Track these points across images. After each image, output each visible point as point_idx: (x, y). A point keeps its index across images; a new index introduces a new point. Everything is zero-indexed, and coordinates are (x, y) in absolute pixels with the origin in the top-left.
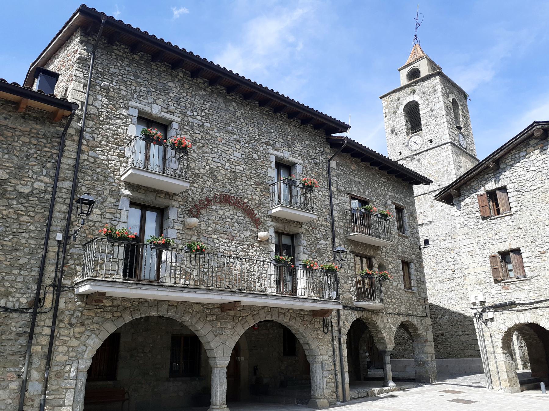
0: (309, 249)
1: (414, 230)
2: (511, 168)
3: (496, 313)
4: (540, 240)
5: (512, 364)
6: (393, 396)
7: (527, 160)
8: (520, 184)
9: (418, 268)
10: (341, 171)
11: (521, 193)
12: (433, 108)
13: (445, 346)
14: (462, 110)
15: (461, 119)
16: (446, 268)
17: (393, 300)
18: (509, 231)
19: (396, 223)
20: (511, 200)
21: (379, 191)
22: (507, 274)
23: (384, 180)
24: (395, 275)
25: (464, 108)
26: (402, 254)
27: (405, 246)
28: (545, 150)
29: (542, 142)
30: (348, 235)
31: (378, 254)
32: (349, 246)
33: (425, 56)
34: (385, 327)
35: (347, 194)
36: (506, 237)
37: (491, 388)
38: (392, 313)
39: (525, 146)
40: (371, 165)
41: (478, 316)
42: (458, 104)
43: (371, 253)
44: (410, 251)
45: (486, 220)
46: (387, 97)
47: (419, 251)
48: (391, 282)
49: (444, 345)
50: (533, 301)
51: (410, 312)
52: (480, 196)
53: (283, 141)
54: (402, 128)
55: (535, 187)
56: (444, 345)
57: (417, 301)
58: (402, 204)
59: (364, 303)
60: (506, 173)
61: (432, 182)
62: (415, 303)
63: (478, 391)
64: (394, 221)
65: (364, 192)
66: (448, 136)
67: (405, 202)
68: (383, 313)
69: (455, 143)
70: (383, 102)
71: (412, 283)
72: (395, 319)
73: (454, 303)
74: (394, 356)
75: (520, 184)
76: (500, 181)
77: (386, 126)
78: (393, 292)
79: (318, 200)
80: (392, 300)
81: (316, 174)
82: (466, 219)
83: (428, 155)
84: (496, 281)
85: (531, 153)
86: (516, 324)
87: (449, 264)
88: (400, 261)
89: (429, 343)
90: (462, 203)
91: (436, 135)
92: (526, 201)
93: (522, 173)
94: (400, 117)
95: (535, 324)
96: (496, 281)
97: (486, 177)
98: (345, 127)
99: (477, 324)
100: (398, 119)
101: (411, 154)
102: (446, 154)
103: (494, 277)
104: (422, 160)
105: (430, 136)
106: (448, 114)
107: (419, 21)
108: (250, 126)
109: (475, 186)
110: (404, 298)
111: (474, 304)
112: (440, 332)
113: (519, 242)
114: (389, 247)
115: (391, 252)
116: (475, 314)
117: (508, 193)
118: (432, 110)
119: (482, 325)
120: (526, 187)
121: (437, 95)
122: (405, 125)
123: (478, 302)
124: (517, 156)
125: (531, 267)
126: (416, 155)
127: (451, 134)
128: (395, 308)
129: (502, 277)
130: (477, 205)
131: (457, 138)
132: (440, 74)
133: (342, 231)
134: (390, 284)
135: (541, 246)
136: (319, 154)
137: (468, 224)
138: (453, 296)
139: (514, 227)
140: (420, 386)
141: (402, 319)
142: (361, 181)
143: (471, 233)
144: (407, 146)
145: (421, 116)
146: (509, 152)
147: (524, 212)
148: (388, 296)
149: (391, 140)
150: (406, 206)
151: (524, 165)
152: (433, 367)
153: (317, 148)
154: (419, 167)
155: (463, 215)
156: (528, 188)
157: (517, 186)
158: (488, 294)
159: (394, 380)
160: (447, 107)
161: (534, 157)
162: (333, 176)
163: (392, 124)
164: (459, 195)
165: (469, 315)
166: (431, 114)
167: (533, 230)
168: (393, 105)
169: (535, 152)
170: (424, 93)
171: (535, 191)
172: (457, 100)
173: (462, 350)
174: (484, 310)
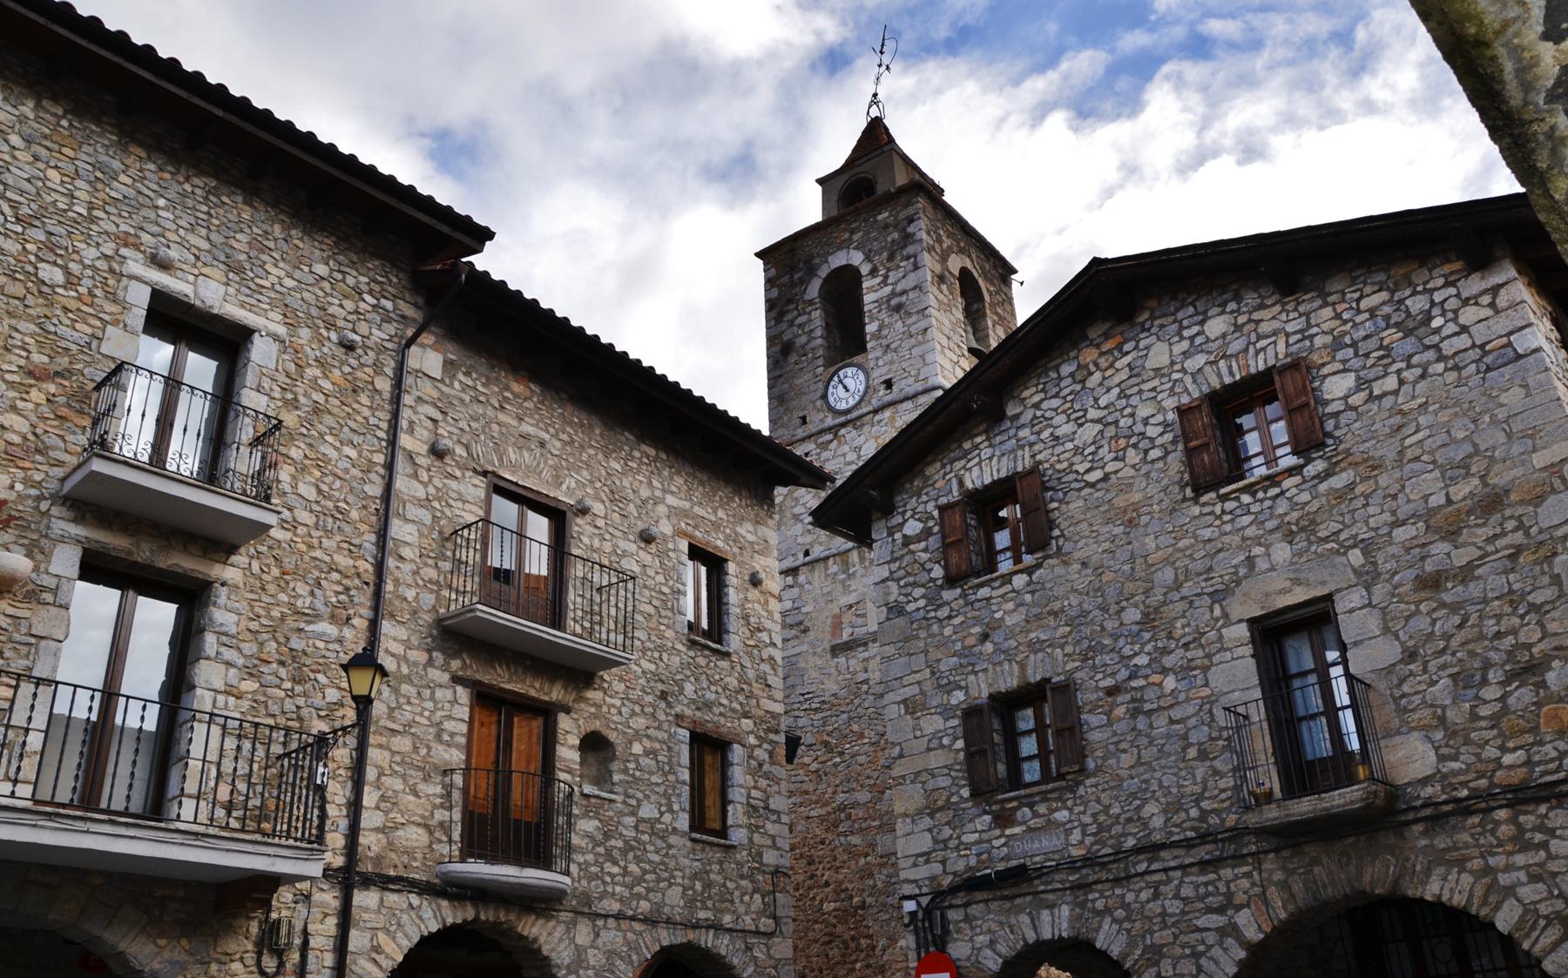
0: (249, 648)
8: (1058, 467)
9: (761, 765)
10: (463, 390)
17: (633, 867)
18: (1023, 624)
24: (654, 779)
26: (698, 709)
29: (1119, 329)
35: (475, 471)
38: (619, 916)
42: (979, 288)
48: (634, 802)
51: (702, 915)
53: (205, 245)
57: (742, 877)
58: (720, 543)
62: (729, 884)
65: (557, 477)
67: (735, 538)
71: (730, 814)
79: (335, 475)
80: (625, 868)
81: (341, 382)
86: (1026, 944)
88: (684, 734)
93: (1067, 429)
94: (810, 313)
97: (967, 445)
105: (885, 369)
108: (56, 167)
109: (936, 477)
113: (1047, 660)
115: (649, 699)
120: (1075, 476)
124: (1054, 375)
128: (639, 897)
130: (934, 542)
136: (368, 316)
141: (666, 937)
150: (736, 550)
151: (1069, 405)
153: (367, 297)
172: (976, 275)
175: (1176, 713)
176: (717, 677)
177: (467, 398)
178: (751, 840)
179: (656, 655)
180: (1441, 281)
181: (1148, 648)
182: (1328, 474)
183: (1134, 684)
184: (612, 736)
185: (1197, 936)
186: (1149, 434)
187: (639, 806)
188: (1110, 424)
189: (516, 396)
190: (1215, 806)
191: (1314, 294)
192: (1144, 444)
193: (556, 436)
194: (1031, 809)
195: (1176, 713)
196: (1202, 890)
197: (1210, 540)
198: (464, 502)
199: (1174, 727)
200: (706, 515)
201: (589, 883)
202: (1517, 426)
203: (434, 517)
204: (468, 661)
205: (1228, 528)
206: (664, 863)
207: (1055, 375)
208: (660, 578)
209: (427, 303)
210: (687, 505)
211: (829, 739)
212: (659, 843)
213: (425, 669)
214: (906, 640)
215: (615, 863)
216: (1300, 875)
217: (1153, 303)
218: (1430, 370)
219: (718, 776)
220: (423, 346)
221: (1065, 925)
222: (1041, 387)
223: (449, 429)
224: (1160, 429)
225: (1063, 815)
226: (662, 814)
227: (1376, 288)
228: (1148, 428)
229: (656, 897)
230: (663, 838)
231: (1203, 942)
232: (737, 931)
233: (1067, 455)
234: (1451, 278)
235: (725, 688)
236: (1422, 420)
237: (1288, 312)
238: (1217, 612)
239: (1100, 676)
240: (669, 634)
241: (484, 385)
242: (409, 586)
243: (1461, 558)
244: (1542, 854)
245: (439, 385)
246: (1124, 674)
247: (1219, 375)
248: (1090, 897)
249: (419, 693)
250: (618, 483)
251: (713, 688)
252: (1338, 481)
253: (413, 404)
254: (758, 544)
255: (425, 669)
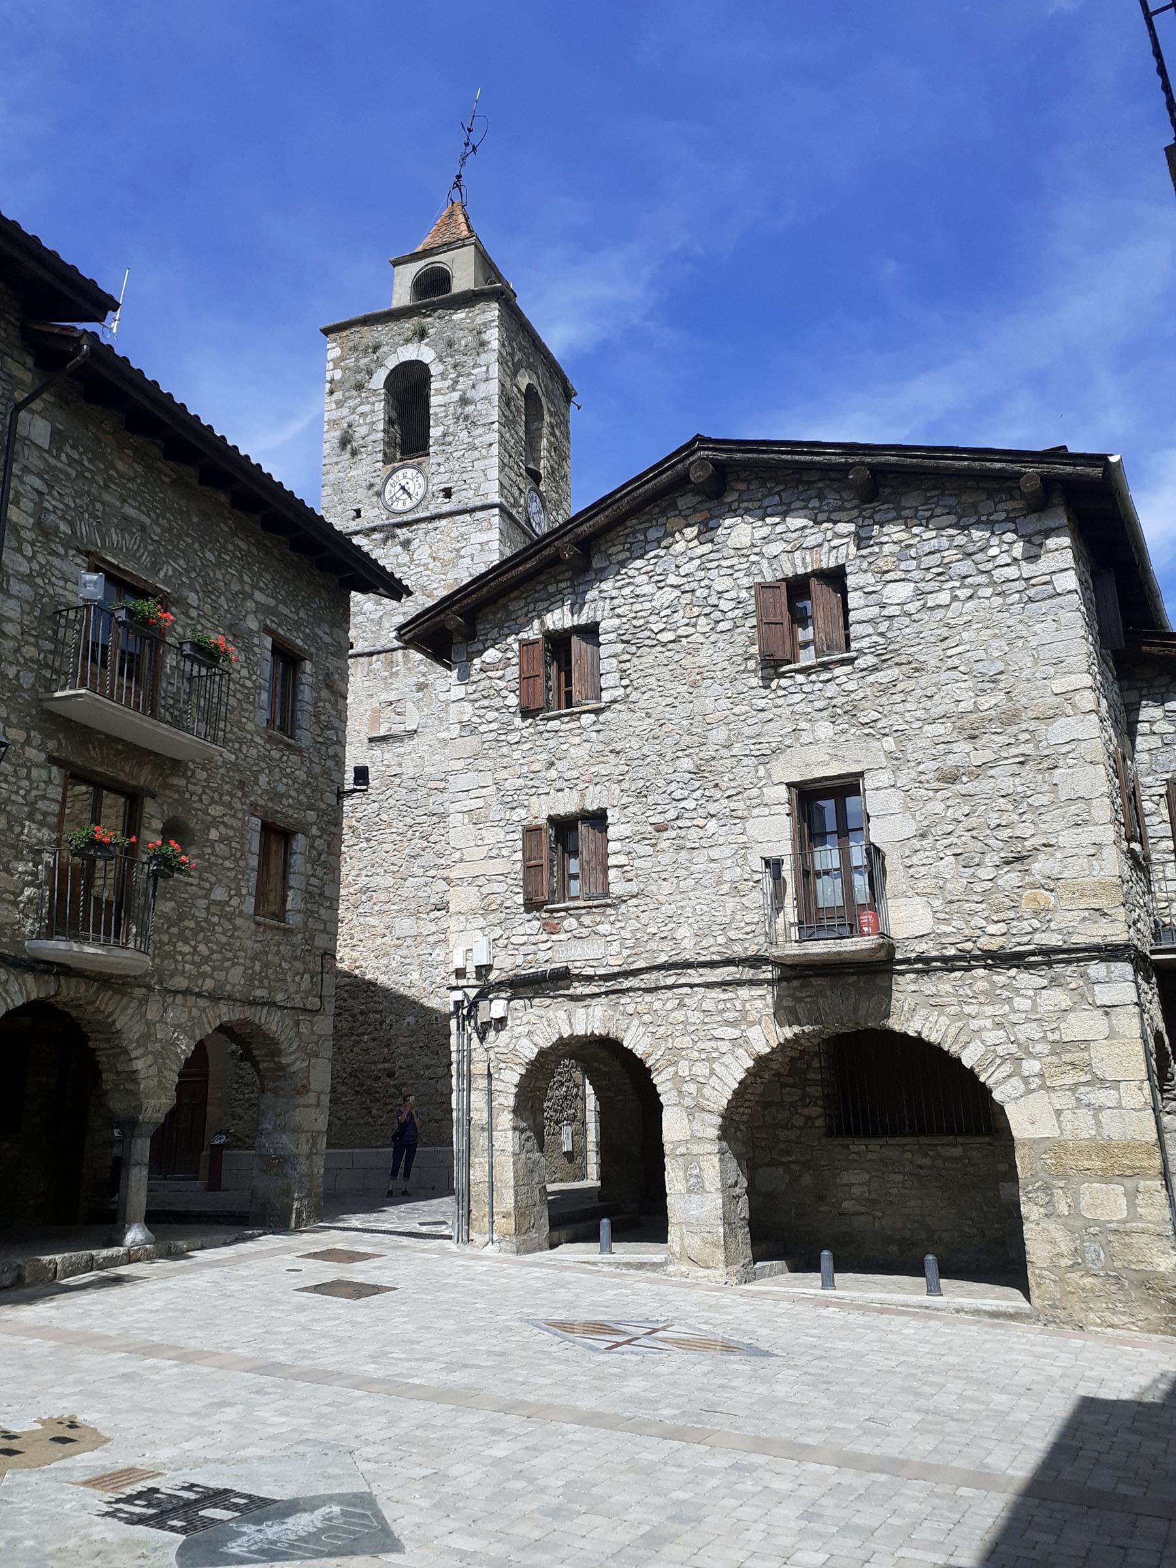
1: (331, 734)
2: (618, 573)
3: (516, 1003)
4: (660, 791)
5: (536, 1163)
6: (119, 1280)
7: (662, 552)
8: (635, 622)
9: (320, 854)
10: (69, 465)
11: (634, 649)
12: (468, 395)
13: (391, 1111)
14: (552, 426)
15: (544, 453)
16: (432, 873)
17: (202, 948)
18: (587, 758)
19: (264, 696)
20: (604, 666)
21: (219, 576)
22: (564, 887)
23: (243, 546)
24: (227, 864)
25: (559, 425)
26: (271, 799)
27: (287, 776)
28: (712, 529)
29: (708, 505)
30: (48, 695)
31: (171, 787)
32: (47, 736)
33: (472, 240)
34: (147, 1037)
35: (78, 550)
36: (575, 774)
37: (465, 1239)
38: (187, 992)
39: (663, 513)
40: (202, 482)
41: (465, 1012)
43: (144, 777)
44: (302, 797)
45: (530, 720)
46: (344, 334)
47: (334, 802)
48: (207, 886)
49: (390, 1107)
50: (617, 969)
51: (258, 993)
52: (525, 644)
54: (373, 437)
55: (670, 636)
56: (390, 1107)
57: (295, 958)
58: (299, 642)
59: (62, 945)
60: (604, 586)
61: (410, 593)
62: (285, 965)
63: (423, 1251)
64: (260, 687)
65: (154, 564)
66: (495, 485)
67: (313, 638)
68: (150, 988)
69: (514, 512)
70: (329, 346)
71: (289, 899)
72: (195, 1012)
73: (438, 980)
74: (239, 1139)
75: (635, 622)
76: (587, 606)
77: (329, 422)
78: (207, 920)
80: (195, 948)
82: (478, 712)
83: (433, 534)
84: (531, 905)
85: (677, 534)
86: (561, 1038)
87: (442, 861)
88: (256, 823)
89: (311, 1098)
90: (476, 661)
91: (465, 476)
92: (643, 674)
93: (646, 589)
94: (373, 404)
95: (611, 1039)
96: (531, 905)
97: (552, 589)
98: (103, 305)
99: (458, 1038)
100: (365, 408)
101: (387, 522)
102: (484, 537)
103: (526, 893)
104: (414, 545)
105: (447, 476)
106: (507, 422)
107: (474, 138)
109: (520, 613)
110: (249, 943)
111: (460, 973)
112: (386, 1065)
113: (605, 792)
114: (222, 771)
115: (227, 787)
116: (459, 1005)
117: (600, 645)
118: (464, 401)
119: (470, 1039)
121: (484, 358)
122: (384, 431)
123: (471, 969)
125: (625, 868)
126: (400, 525)
127: (506, 482)
128: (204, 975)
129: (546, 894)
130: (513, 672)
131: (522, 502)
132: (505, 298)
133: (27, 679)
134: (201, 893)
135: (660, 809)
137: (482, 728)
138: (440, 959)
139: (601, 747)
140: (251, 1238)
141: (226, 1013)
142: (148, 521)
143: (486, 757)
144: (379, 494)
145: (432, 411)
146: (619, 521)
147: (631, 706)
148: (182, 932)
149: (338, 468)
151: (651, 567)
152: (311, 1176)
154: (404, 565)
155: (471, 697)
156: (653, 636)
157: (627, 626)
158: (502, 942)
159: (153, 1219)
160: (506, 400)
161: (680, 547)
162: (26, 469)
163: (347, 420)
164: (470, 635)
165: (432, 1003)
166: (459, 410)
167: (648, 760)
168: (357, 360)
169: (687, 531)
170: (450, 344)
171: (670, 646)
172: (540, 393)
173: (436, 1121)
174: (482, 995)
175: (715, 853)
176: (288, 770)
177: (74, 474)
178: (306, 923)
179: (237, 746)
180: (1003, 515)
181: (697, 794)
182: (875, 669)
183: (679, 823)
184: (192, 824)
185: (713, 1044)
186: (722, 607)
187: (211, 889)
188: (687, 592)
189: (121, 475)
190: (741, 936)
191: (891, 506)
192: (717, 615)
193: (156, 522)
194: (577, 919)
195: (715, 853)
196: (721, 1006)
197: (762, 710)
198: (66, 581)
199: (712, 865)
200: (290, 615)
201: (162, 962)
202: (1044, 654)
203: (36, 593)
204: (63, 742)
205: (780, 701)
206: (229, 944)
207: (642, 538)
208: (244, 672)
209: (36, 365)
210: (272, 602)
211: (356, 824)
212: (229, 926)
213: (22, 748)
214: (476, 756)
215: (187, 942)
216: (806, 1003)
217: (742, 486)
218: (980, 593)
219: (281, 863)
220: (32, 412)
221: (597, 1024)
222: (628, 546)
223: (54, 503)
224: (732, 604)
225: (603, 928)
226: (231, 897)
227: (946, 511)
228: (722, 601)
229: (220, 976)
230: (229, 920)
231: (717, 1049)
232: (286, 1008)
233: (644, 614)
234: (1012, 515)
235: (295, 780)
236: (965, 635)
237: (864, 518)
238: (761, 773)
239: (651, 813)
240: (250, 726)
241: (89, 460)
242: (11, 663)
243: (978, 758)
244: (1007, 1007)
245: (47, 456)
246: (672, 814)
247: (794, 564)
248: (623, 1001)
249: (15, 771)
250: (212, 575)
251: (285, 780)
252: (883, 677)
253: (19, 473)
254: (333, 646)
255: (22, 748)
